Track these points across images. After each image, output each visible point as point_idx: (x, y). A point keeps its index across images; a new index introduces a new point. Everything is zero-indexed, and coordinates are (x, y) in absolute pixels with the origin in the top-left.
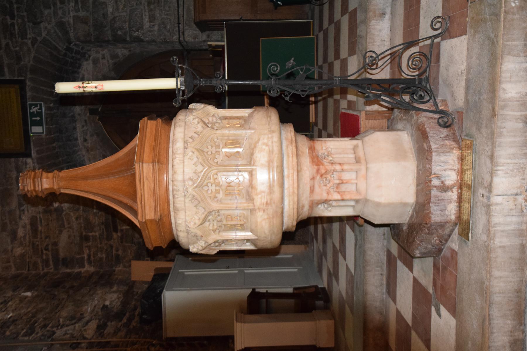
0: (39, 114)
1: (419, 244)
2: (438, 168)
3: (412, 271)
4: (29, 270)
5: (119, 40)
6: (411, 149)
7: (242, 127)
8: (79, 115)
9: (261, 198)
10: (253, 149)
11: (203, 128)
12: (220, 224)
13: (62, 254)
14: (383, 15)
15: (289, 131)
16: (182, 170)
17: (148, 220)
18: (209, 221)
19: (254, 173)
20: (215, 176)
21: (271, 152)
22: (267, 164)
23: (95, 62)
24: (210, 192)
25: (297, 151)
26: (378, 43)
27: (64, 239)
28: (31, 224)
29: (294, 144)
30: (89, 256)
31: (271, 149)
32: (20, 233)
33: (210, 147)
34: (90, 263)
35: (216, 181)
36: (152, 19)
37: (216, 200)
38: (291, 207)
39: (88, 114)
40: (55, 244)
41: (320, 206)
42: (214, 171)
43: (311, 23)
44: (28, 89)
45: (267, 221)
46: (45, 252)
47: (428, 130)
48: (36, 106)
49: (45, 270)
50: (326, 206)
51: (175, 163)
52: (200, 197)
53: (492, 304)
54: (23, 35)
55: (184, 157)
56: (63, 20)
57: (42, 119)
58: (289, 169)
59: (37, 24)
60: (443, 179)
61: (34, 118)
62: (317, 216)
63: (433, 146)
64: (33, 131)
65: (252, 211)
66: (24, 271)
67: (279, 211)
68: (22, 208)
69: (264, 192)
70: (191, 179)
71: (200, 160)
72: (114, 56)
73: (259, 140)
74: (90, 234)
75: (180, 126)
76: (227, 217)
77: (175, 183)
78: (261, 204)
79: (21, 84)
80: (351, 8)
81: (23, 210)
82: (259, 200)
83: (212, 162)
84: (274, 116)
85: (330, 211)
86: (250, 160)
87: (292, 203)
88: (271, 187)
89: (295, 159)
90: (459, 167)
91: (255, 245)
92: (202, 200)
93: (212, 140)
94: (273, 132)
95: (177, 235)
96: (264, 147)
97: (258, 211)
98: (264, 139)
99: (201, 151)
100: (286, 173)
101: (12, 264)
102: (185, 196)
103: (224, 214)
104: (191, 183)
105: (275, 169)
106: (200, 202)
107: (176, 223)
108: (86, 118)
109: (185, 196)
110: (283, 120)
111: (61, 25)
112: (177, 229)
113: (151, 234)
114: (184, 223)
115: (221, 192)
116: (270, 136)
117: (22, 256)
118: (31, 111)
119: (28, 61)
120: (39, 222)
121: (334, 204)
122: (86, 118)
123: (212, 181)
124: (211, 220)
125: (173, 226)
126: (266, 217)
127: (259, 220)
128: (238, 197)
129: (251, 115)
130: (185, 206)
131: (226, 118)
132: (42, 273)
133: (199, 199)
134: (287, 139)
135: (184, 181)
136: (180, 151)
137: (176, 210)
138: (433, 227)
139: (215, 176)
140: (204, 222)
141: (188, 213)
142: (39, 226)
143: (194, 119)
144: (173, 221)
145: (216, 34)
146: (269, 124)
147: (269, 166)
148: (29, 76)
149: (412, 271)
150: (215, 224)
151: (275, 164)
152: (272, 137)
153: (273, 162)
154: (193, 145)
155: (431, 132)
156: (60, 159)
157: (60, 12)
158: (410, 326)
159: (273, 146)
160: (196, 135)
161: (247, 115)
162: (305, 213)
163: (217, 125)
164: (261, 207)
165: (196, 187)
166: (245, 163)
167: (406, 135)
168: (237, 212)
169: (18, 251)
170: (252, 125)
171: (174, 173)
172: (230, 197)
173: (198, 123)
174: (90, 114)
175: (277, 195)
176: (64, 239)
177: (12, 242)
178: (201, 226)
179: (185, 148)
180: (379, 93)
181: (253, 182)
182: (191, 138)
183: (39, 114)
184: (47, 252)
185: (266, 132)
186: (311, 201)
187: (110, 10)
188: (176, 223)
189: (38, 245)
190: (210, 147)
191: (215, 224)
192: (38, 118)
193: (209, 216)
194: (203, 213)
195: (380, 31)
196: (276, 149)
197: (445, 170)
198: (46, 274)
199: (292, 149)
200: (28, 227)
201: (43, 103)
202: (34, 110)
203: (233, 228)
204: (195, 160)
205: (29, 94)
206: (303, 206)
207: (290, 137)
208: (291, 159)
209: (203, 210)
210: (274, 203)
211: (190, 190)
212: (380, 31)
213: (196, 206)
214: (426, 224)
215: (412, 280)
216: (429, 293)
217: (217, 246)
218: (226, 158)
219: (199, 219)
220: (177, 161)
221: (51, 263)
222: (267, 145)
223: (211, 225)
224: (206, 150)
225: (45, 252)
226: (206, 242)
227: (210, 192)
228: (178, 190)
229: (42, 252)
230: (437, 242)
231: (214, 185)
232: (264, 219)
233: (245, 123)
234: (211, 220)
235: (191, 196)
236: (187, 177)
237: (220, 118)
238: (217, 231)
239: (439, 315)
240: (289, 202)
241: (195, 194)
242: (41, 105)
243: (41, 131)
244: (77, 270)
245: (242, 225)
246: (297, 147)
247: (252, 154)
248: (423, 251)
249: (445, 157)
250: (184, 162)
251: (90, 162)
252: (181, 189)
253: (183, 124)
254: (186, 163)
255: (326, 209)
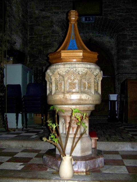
0: (89, 20)
1: (49, 157)
2: (79, 163)
3: (35, 157)
4: (29, 15)
6: (85, 154)
7: (95, 90)
8: (89, 35)
9: (69, 96)
10: (87, 93)
11: (95, 75)
12: (58, 81)
14: (133, 148)
15: (92, 108)
16: (79, 67)
17: (61, 54)
18: (60, 77)
19: (78, 94)
20: (77, 79)
21: (86, 100)
22: (81, 98)
24: (71, 77)
25: (86, 111)
26: (122, 146)
28: (47, 16)
29: (88, 110)
30: (34, 37)
31: (87, 100)
32: (44, 13)
33: (88, 77)
34: (31, 38)
35: (75, 80)
37: (68, 79)
38: (64, 108)
39: (89, 38)
40: (39, 25)
41: (63, 120)
42: (79, 79)
44: (99, 16)
45: (59, 99)
46: (36, 21)
47: (93, 160)
48: (93, 19)
49: (29, 22)
50: (64, 122)
51: (82, 64)
52: (69, 73)
55: (84, 68)
56: (125, 31)
57: (87, 21)
58: (79, 107)
60: (75, 165)
61: (88, 18)
62: (59, 119)
63: (87, 162)
64: (83, 18)
65: (64, 93)
66: (29, 13)
67: (63, 103)
68: (53, 13)
69: (71, 97)
70: (76, 70)
71: (83, 73)
73: (90, 96)
74: (42, 38)
75: (95, 67)
76: (61, 84)
77: (75, 64)
78: (66, 96)
79: (101, 14)
80: (134, 137)
81: (52, 14)
82: (68, 96)
83: (82, 78)
84: (98, 102)
85: (61, 124)
86: (83, 92)
87: (66, 108)
88: (71, 100)
89: (82, 110)
90: (79, 171)
91: (49, 94)
92: (68, 74)
93: (90, 78)
94: (93, 101)
95: (54, 65)
96: (88, 98)
97: (63, 95)
99: (86, 73)
100: (78, 106)
101: (32, 9)
102: (70, 68)
103: (62, 82)
104: (75, 70)
105: (79, 102)
106: (67, 73)
107: (59, 64)
108: (87, 38)
109: (70, 68)
110: (96, 106)
112: (56, 65)
114: (59, 67)
115: (71, 81)
116: (92, 100)
117: (35, 13)
118: (91, 17)
120: (48, 19)
121: (64, 125)
122: (87, 38)
123: (75, 78)
124: (60, 77)
125: (58, 64)
126: (61, 98)
127: (60, 96)
128: (69, 87)
129: (99, 94)
130: (66, 68)
131: (98, 84)
132: (28, 20)
133: (68, 73)
134: (90, 107)
135: (75, 67)
136: (86, 66)
137: (64, 64)
138: (56, 162)
139: (77, 79)
140: (59, 75)
141: (63, 69)
142: (46, 19)
143: (98, 72)
144: (59, 63)
146: (96, 100)
147: (81, 99)
148: (104, 17)
149: (35, 157)
150: (58, 79)
151: (81, 102)
152: (91, 101)
153: (82, 101)
154: (89, 71)
155: (92, 161)
157: (128, 29)
158: (12, 158)
159: (88, 101)
160: (92, 72)
161: (99, 92)
162: (61, 114)
163: (95, 81)
164: (65, 96)
165: (73, 72)
166: (82, 90)
167: (90, 153)
168: (63, 87)
169: (37, 12)
170: (95, 94)
171: (78, 64)
172: (69, 84)
173: (97, 73)
174: (89, 39)
175: (70, 102)
177: (40, 10)
178: (58, 73)
179: (87, 68)
181: (74, 93)
182: (91, 70)
183: (89, 20)
184: (36, 22)
185: (93, 99)
186: (66, 116)
187: (130, 48)
188: (59, 64)
189: (39, 19)
190: (88, 77)
191: (58, 79)
192: (88, 20)
193: (62, 76)
194: (63, 74)
195: (127, 147)
196: (87, 102)
197: (78, 166)
198: (27, 22)
199: (86, 109)
200: (46, 15)
201: (94, 22)
202: (91, 18)
203: (57, 86)
204: (83, 72)
205: (97, 17)
206: (63, 113)
207: (90, 108)
208: (83, 108)
209: (64, 74)
210: (66, 101)
211: (72, 69)
212: (127, 147)
213: (66, 72)
214: (57, 159)
215: (31, 157)
216: (28, 162)
217: (49, 80)
218: (84, 83)
219: (61, 73)
220: (83, 65)
221: (32, 23)
222: (88, 99)
223: (58, 78)
224: (87, 76)
225: (36, 21)
226: (51, 76)
227: (71, 77)
228: (72, 65)
229: (35, 20)
230: (50, 164)
231: (73, 78)
232: (60, 98)
233: (96, 92)
234: (60, 77)
235: (69, 70)
236: (77, 68)
237: (98, 82)
238: (55, 80)
239: (21, 165)
240: (66, 107)
241: (71, 71)
242: (93, 21)
243: (83, 21)
244: (28, 33)
245: (58, 89)
246: (87, 111)
247: (85, 93)
248: (46, 159)
249: (83, 166)
250: (82, 67)
251: (80, 35)
252: (72, 66)
253: (96, 68)
254: (82, 68)
255: (62, 122)
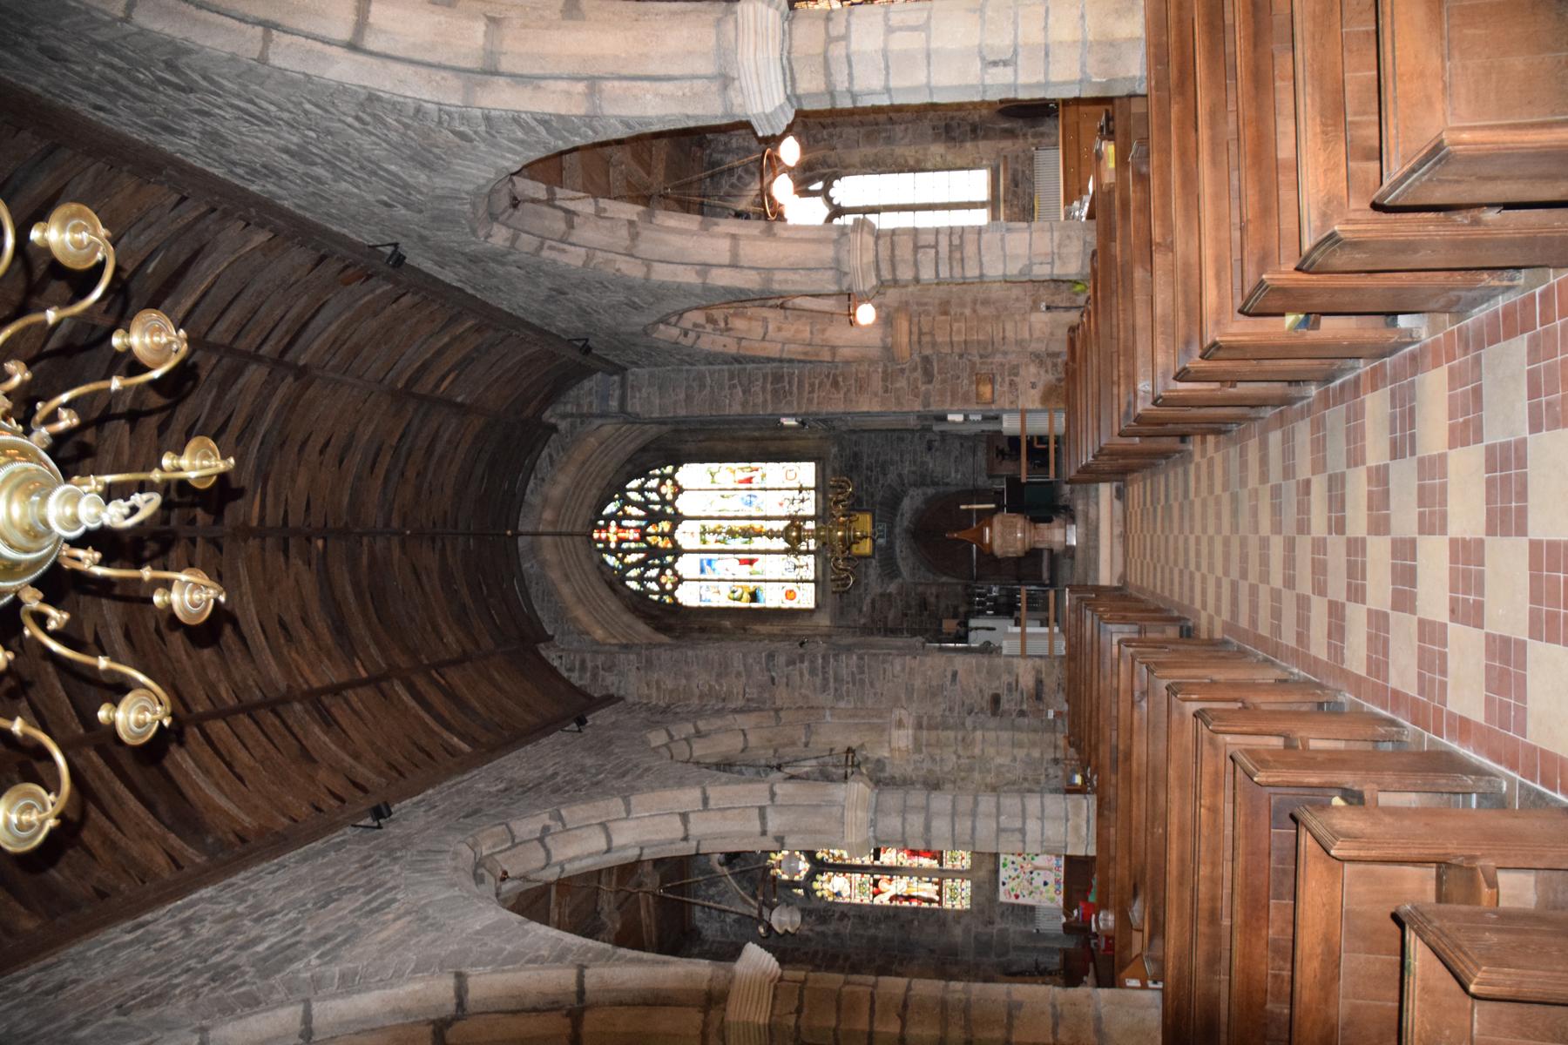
5: (935, 484)
13: (890, 625)
23: (912, 498)
27: (891, 616)
32: (865, 609)
36: (957, 471)
40: (886, 617)
43: (1041, 556)
53: (586, 94)
54: (877, 481)
59: (885, 475)
72: (924, 494)
98: (758, 727)
111: (900, 475)
113: (1250, 331)
119: (878, 498)
145: (998, 481)
156: (1461, 420)
176: (891, 616)
180: (226, 813)
